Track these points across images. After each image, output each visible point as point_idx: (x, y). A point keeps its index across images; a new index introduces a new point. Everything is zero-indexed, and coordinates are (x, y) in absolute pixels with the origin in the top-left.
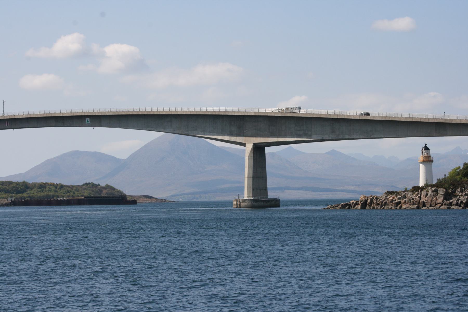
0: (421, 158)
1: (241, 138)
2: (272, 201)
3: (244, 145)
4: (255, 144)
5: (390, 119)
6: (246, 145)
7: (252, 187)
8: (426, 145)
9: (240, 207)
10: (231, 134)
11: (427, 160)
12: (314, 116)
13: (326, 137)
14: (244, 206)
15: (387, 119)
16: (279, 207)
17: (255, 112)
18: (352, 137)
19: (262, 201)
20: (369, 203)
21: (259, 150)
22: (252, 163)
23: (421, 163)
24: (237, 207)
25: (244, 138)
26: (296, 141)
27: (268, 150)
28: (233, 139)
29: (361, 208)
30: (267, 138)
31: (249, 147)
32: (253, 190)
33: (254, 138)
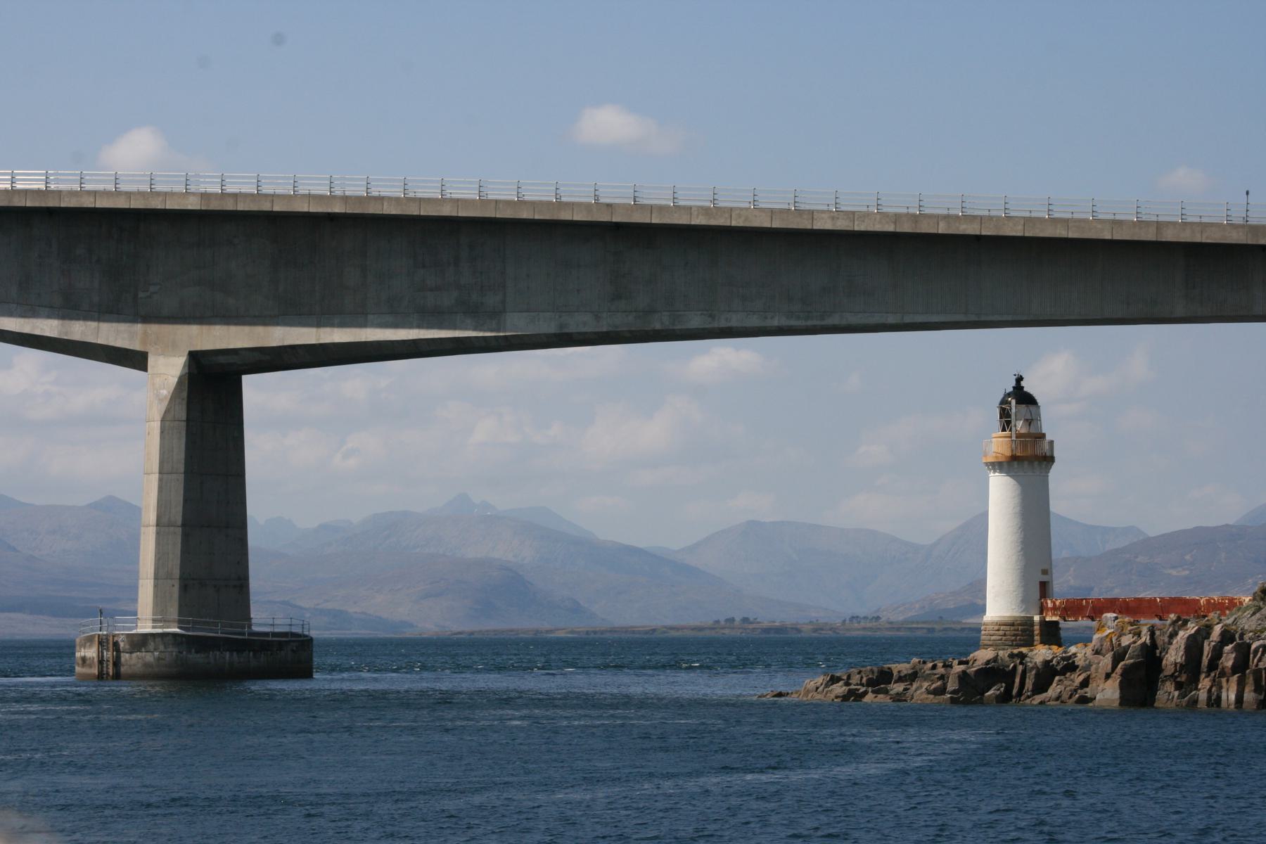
0: (998, 444)
1: (123, 327)
2: (281, 645)
3: (137, 360)
4: (195, 358)
5: (942, 229)
6: (151, 361)
7: (177, 572)
8: (1020, 379)
9: (117, 676)
10: (70, 308)
11: (1029, 452)
12: (525, 214)
13: (580, 322)
14: (138, 668)
15: (925, 228)
16: (307, 674)
17: (205, 196)
18: (723, 324)
19: (226, 649)
20: (1182, 668)
21: (211, 398)
22: (179, 454)
23: (998, 466)
24: (101, 676)
25: (139, 327)
26: (415, 342)
27: (255, 388)
28: (80, 330)
29: (1125, 700)
30: (260, 330)
31: (168, 369)
32: (185, 587)
33: (194, 329)
